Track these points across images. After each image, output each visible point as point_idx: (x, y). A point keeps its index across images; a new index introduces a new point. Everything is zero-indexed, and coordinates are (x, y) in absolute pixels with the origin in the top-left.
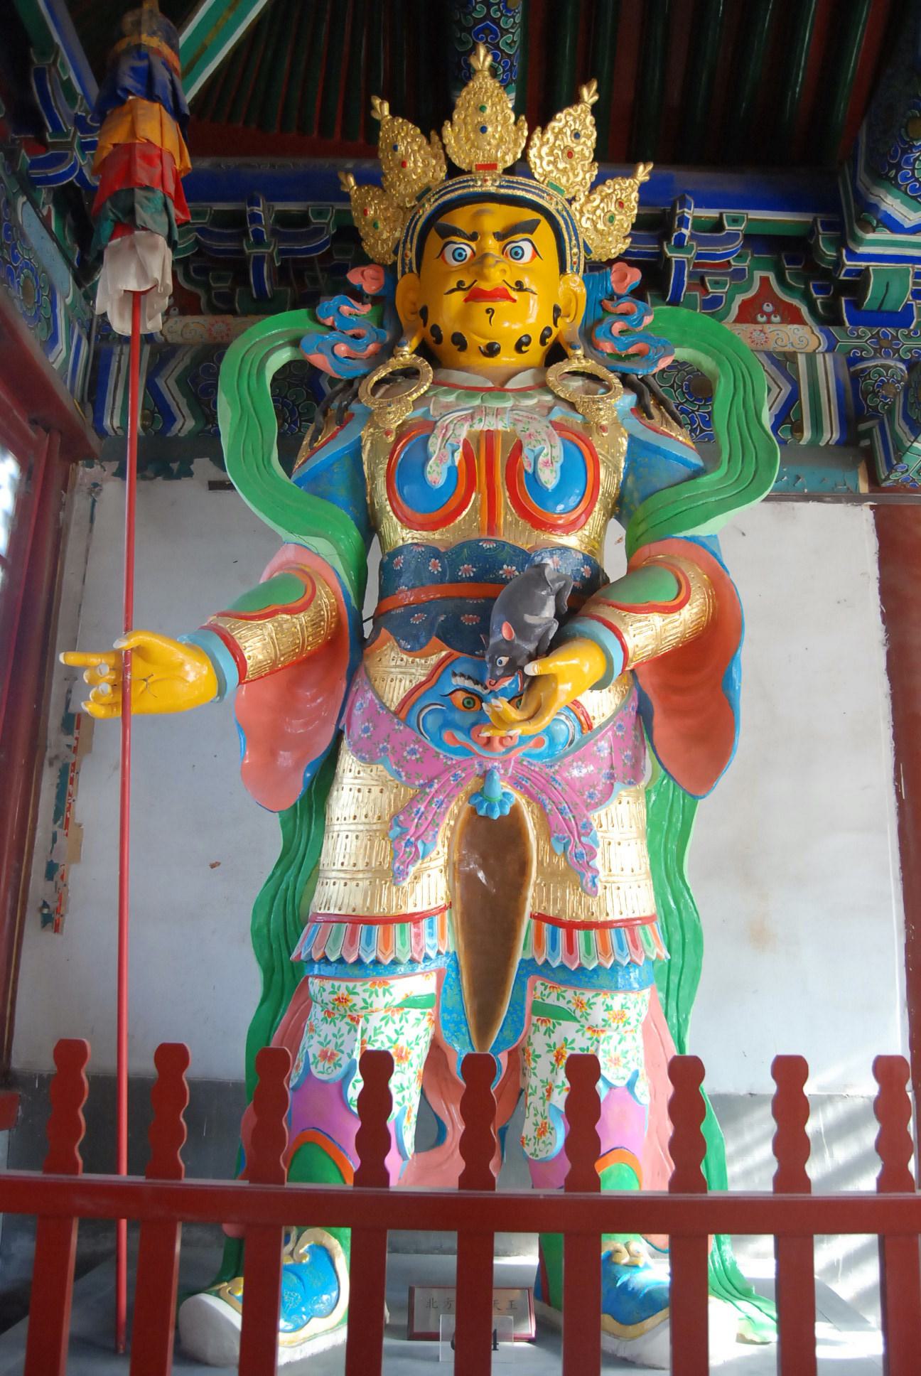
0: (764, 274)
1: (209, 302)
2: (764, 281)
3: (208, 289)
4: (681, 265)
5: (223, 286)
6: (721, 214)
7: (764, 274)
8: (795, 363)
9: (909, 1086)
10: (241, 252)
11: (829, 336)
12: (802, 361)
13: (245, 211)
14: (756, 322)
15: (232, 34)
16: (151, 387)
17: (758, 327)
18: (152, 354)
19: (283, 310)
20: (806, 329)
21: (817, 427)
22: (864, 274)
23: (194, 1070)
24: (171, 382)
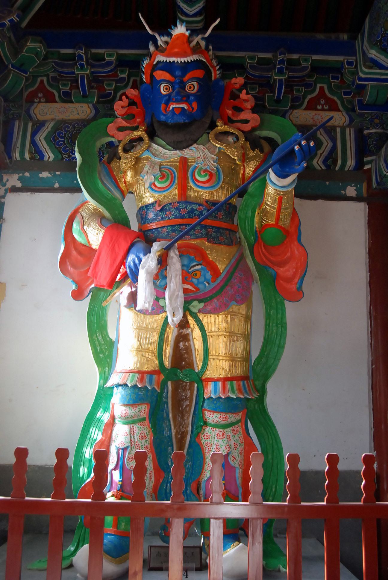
0: (322, 85)
1: (60, 96)
2: (322, 88)
3: (59, 91)
4: (280, 81)
5: (67, 89)
6: (300, 57)
7: (322, 85)
8: (335, 131)
9: (385, 487)
10: (74, 73)
11: (350, 116)
12: (338, 130)
13: (75, 54)
14: (316, 109)
15: (31, 19)
16: (33, 143)
17: (317, 112)
18: (33, 126)
19: (278, 115)
20: (339, 113)
21: (344, 161)
22: (364, 87)
23: (31, 460)
24: (42, 139)
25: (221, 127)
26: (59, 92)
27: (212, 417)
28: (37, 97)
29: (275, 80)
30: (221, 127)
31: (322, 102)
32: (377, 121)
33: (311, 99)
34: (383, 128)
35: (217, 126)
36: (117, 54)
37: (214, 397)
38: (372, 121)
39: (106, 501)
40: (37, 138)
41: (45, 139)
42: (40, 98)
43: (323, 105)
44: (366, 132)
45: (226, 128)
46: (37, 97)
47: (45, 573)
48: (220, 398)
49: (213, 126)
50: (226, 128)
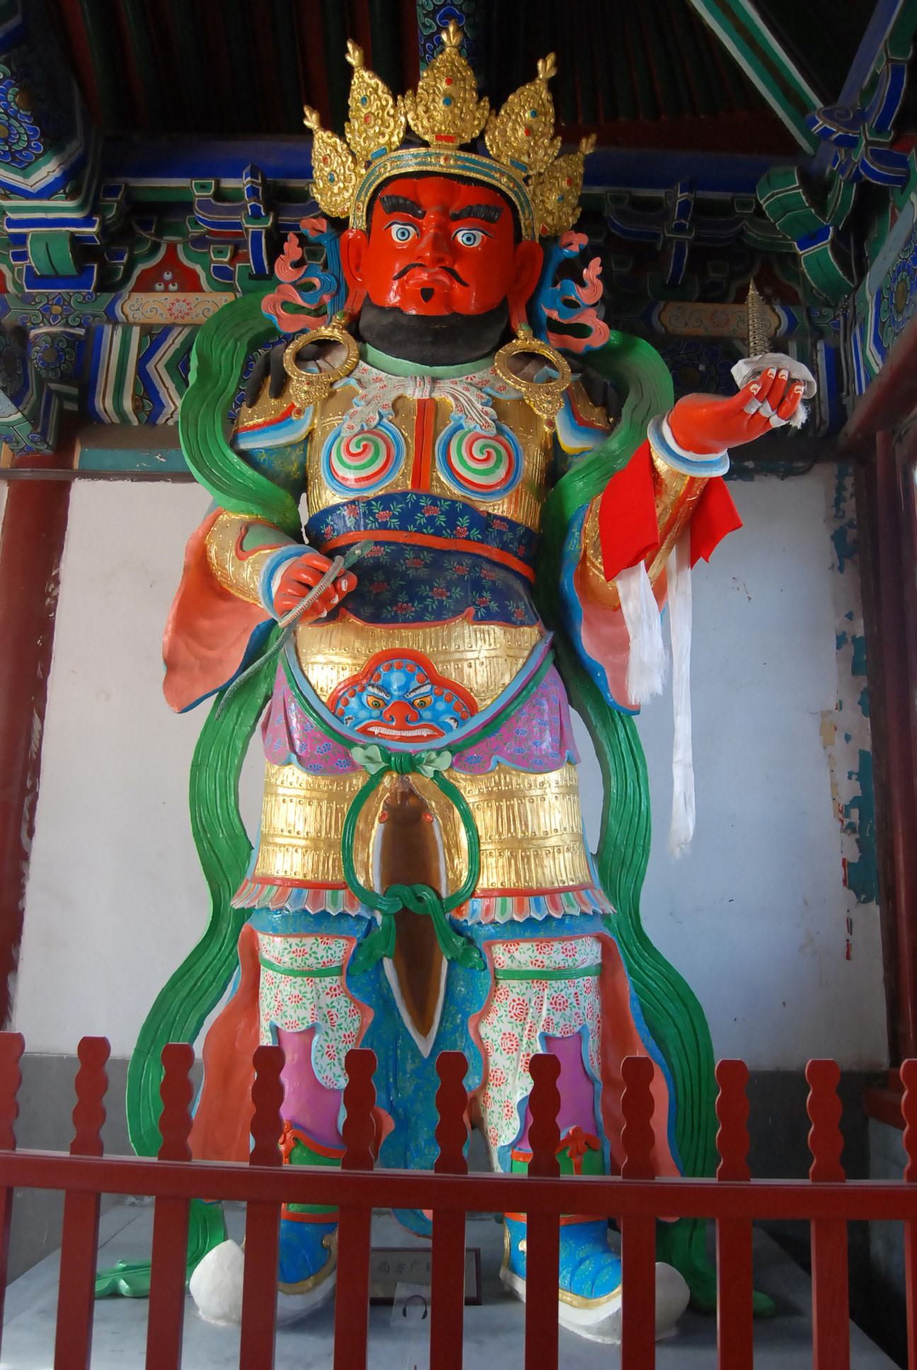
6: (733, 199)
15: (780, 120)
25: (524, 339)
26: (206, 269)
27: (273, 947)
28: (161, 279)
29: (667, 241)
30: (524, 339)
31: (168, 276)
32: (57, 309)
33: (143, 272)
34: (67, 324)
35: (517, 338)
36: (130, 191)
37: (501, 922)
38: (46, 309)
39: (658, 1179)
40: (150, 367)
41: (167, 366)
42: (166, 284)
43: (166, 284)
44: (33, 333)
45: (536, 345)
46: (161, 279)
47: (147, 1301)
48: (512, 921)
49: (509, 335)
50: (536, 345)
